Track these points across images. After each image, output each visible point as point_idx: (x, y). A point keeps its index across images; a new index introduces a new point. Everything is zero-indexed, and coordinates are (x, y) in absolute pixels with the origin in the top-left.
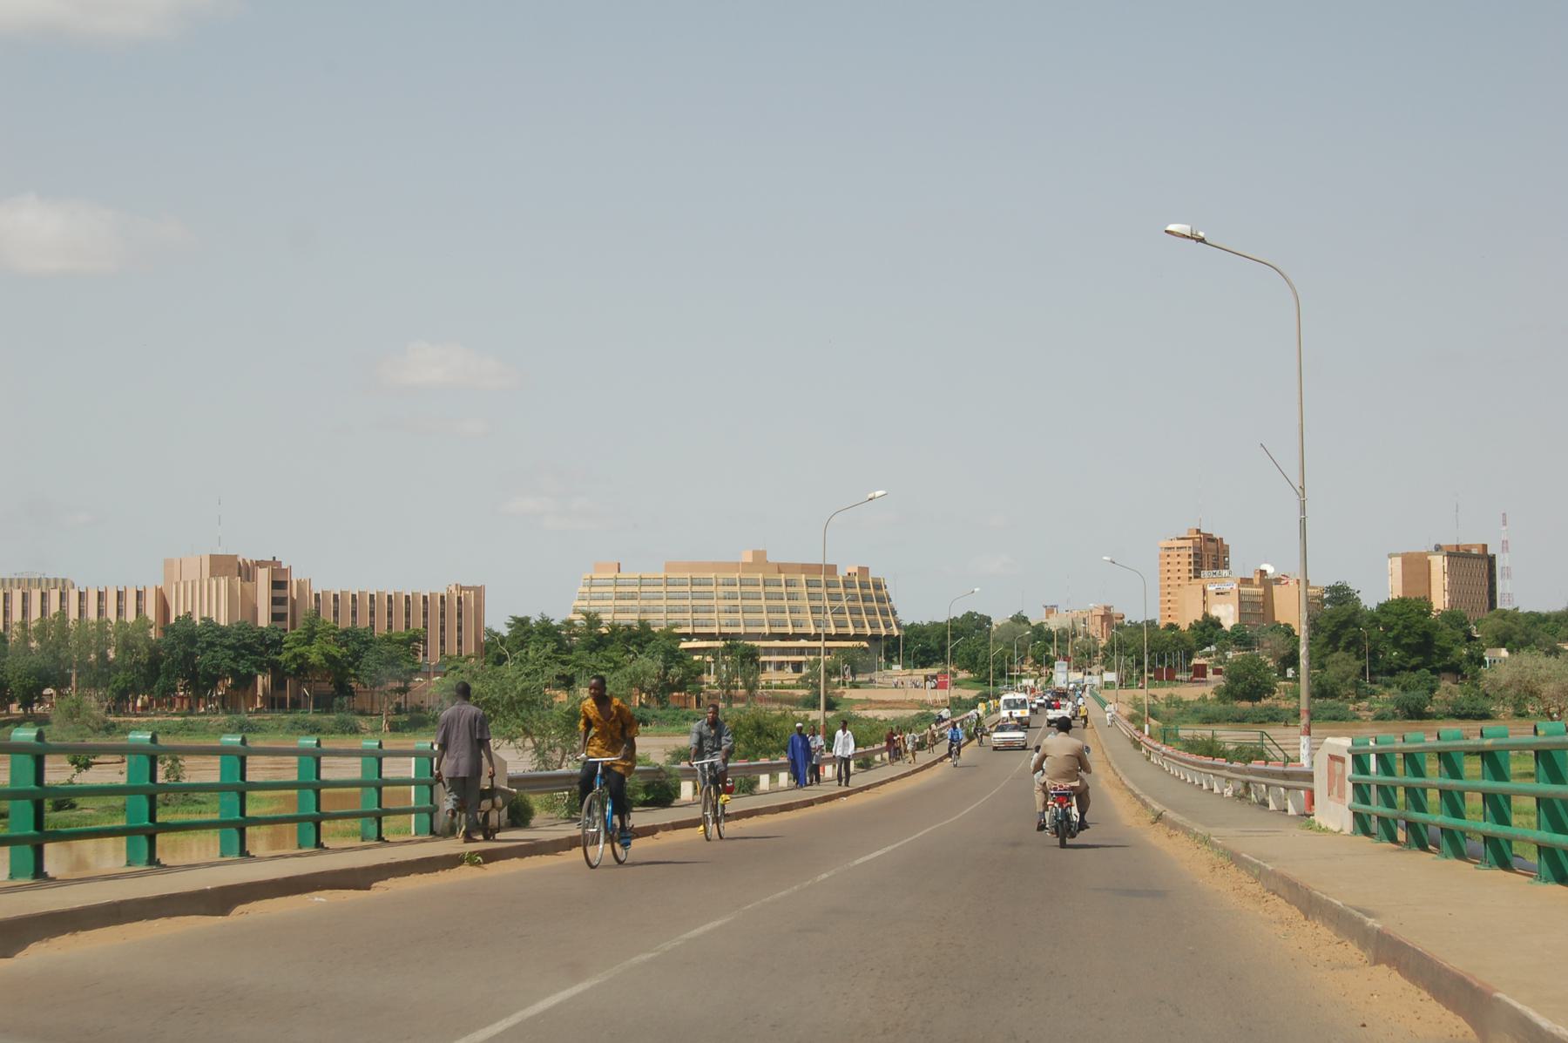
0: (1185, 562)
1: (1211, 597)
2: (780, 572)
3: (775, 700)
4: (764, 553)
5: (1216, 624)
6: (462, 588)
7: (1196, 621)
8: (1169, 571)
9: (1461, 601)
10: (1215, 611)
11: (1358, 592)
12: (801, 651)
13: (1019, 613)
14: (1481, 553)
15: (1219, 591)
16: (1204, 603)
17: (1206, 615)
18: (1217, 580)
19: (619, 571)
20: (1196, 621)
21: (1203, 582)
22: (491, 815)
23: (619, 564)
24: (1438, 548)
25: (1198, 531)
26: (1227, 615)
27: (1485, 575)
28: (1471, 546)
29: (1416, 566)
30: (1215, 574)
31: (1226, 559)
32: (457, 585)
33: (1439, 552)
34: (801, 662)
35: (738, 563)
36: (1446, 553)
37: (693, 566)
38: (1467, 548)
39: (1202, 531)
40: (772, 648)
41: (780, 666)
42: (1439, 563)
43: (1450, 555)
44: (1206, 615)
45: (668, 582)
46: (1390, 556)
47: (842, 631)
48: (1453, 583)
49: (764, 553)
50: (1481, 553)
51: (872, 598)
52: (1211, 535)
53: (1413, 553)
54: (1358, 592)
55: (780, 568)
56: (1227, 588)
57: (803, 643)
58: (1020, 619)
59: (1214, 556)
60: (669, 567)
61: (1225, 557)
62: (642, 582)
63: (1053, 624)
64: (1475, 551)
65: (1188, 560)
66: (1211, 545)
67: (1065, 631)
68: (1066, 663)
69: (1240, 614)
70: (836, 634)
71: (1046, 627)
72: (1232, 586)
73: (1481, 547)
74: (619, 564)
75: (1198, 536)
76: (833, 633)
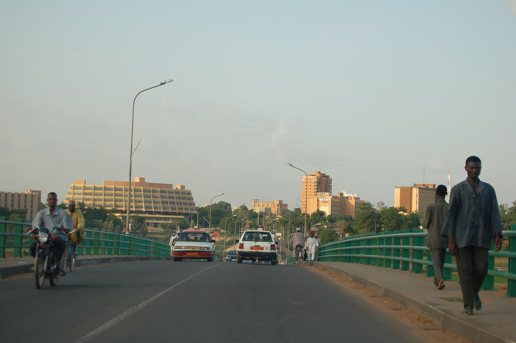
0: (313, 187)
1: (320, 203)
2: (150, 186)
3: (152, 238)
4: (144, 179)
5: (322, 214)
6: (33, 191)
7: (314, 212)
8: (310, 185)
9: (423, 207)
10: (322, 209)
11: (374, 205)
12: (158, 219)
13: (243, 205)
14: (433, 188)
15: (324, 201)
16: (318, 205)
17: (318, 210)
18: (323, 197)
19: (85, 184)
20: (314, 212)
21: (318, 197)
22: (413, 189)
23: (85, 181)
24: (415, 186)
25: (319, 173)
26: (327, 209)
27: (434, 197)
28: (429, 185)
29: (406, 193)
30: (322, 194)
31: (331, 184)
32: (31, 190)
33: (415, 187)
34: (157, 223)
35: (134, 182)
36: (418, 188)
37: (115, 183)
38: (427, 186)
39: (321, 173)
40: (155, 217)
41: (156, 225)
42: (415, 192)
43: (420, 188)
44: (318, 210)
45: (106, 189)
46: (396, 188)
47: (166, 211)
48: (420, 200)
49: (144, 179)
50: (433, 188)
51: (166, 191)
52: (325, 174)
53: (405, 187)
54: (374, 205)
55: (150, 185)
56: (327, 200)
57: (158, 216)
58: (244, 208)
59: (326, 183)
60: (106, 182)
61: (330, 184)
62: (95, 188)
63: (257, 210)
64: (430, 187)
65: (314, 188)
66: (324, 179)
67: (262, 213)
68: (262, 229)
69: (331, 210)
70: (154, 211)
71: (254, 211)
72: (329, 199)
73: (433, 185)
74: (85, 181)
75: (319, 174)
76: (170, 212)
